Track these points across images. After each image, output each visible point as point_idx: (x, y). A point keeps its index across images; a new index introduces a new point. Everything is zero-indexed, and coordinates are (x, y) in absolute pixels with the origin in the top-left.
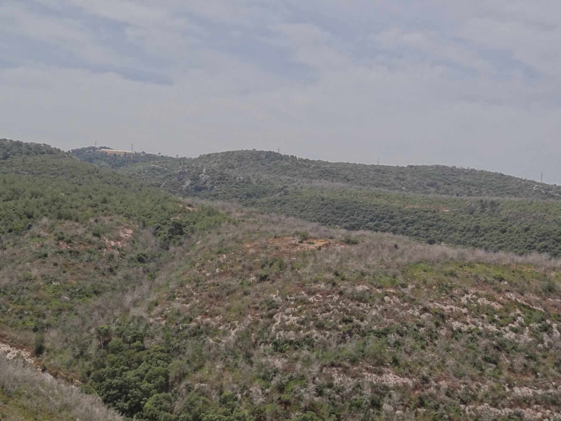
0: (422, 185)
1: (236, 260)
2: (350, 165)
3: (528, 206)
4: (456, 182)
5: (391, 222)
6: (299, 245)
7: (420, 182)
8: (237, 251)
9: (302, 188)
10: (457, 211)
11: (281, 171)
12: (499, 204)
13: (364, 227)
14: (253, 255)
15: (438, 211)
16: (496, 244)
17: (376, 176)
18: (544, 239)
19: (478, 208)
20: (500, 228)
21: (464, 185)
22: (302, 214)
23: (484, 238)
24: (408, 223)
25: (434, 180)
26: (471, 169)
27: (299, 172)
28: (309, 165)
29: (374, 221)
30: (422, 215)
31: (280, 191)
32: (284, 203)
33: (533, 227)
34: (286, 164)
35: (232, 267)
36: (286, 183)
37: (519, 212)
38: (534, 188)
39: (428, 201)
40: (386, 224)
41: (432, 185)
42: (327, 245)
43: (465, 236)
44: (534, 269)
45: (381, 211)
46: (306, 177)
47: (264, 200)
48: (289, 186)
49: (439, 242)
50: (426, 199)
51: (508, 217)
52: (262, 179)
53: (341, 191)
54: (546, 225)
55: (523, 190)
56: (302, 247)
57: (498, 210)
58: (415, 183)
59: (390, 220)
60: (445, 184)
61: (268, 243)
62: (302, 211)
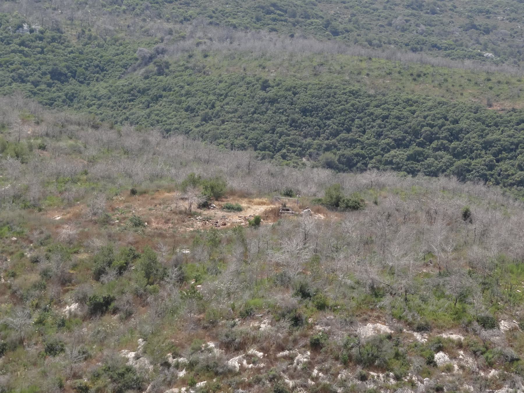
1: (22, 255)
5: (454, 149)
6: (200, 214)
8: (26, 231)
9: (206, 56)
11: (147, 8)
13: (380, 161)
17: (413, 20)
22: (208, 127)
24: (500, 152)
27: (198, 10)
29: (407, 146)
31: (146, 64)
32: (157, 98)
42: (276, 214)
45: (425, 117)
48: (171, 48)
53: (315, 64)
56: (208, 219)
59: (451, 141)
61: (113, 209)
62: (206, 119)
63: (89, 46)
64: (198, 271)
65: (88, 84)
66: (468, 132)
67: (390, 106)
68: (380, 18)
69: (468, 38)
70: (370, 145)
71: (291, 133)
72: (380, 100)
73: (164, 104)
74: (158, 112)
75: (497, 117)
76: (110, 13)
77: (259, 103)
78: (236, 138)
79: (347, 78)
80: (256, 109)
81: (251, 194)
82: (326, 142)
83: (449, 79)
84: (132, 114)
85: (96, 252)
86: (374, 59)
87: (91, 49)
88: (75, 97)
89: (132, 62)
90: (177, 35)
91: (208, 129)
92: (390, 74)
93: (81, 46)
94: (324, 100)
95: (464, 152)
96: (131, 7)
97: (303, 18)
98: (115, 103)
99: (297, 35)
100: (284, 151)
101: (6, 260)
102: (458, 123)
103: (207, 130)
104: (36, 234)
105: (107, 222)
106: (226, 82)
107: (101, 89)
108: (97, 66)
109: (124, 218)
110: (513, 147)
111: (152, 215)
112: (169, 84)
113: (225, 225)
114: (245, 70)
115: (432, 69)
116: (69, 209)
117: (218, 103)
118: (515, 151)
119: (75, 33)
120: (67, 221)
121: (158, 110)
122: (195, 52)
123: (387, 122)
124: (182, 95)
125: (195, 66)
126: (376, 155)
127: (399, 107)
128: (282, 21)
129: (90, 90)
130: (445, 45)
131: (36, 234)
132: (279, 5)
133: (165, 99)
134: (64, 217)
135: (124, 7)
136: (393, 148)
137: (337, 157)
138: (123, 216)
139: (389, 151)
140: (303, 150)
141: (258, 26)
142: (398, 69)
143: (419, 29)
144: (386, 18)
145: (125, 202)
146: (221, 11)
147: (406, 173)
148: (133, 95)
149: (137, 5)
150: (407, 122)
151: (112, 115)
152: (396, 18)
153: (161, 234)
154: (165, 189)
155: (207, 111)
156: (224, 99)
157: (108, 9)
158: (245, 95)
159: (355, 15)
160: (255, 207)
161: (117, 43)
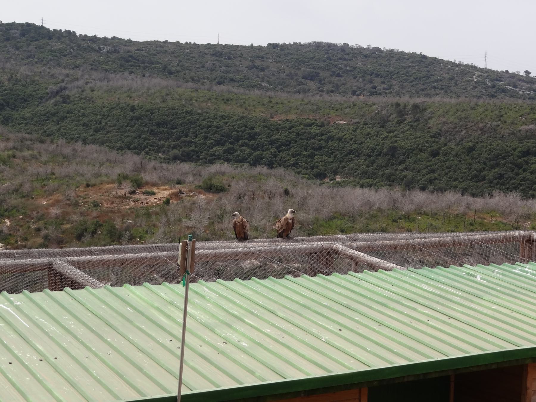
0: (296, 78)
1: (29, 227)
2: (170, 45)
3: (471, 112)
4: (350, 71)
5: (253, 145)
6: (131, 198)
7: (290, 73)
8: (28, 212)
9: (93, 91)
10: (358, 123)
11: (51, 60)
12: (425, 109)
13: (207, 154)
14: (57, 218)
15: (329, 123)
16: (424, 175)
17: (217, 64)
18: (497, 165)
19: (393, 116)
20: (429, 149)
21: (363, 76)
22: (98, 136)
23: (404, 165)
24: (280, 146)
25: (314, 68)
26: (373, 48)
27: (83, 60)
28: (99, 48)
29: (223, 144)
30: (303, 131)
31: (55, 97)
32: (64, 118)
33: (480, 145)
34: (59, 46)
35: (26, 239)
36: (63, 81)
37: (457, 121)
38: (474, 77)
39: (309, 106)
40: (244, 148)
41: (311, 77)
42: (177, 196)
43: (375, 164)
44: (499, 219)
45: (233, 126)
46: (96, 69)
47: (27, 112)
48: (70, 86)
49: (332, 176)
50: (307, 104)
51: (440, 130)
52: (18, 75)
53: (163, 94)
54: (500, 142)
55: (457, 81)
56: (137, 200)
57: (425, 120)
58: (283, 75)
59: (250, 141)
60: (332, 76)
61: (78, 196)
62: (97, 131)
63: (16, 86)
64: (140, 233)
65: (17, 110)
66: (260, 135)
67: (212, 120)
68: (197, 63)
69: (252, 74)
70: (201, 144)
71: (151, 138)
72: (205, 116)
73: (68, 122)
74: (65, 127)
75: (277, 125)
76: (28, 64)
77: (129, 120)
78: (117, 143)
79: (184, 103)
80: (128, 124)
81: (158, 184)
82: (173, 143)
83: (246, 102)
84: (49, 129)
85: (75, 223)
86: (199, 90)
87: (18, 88)
88: (9, 119)
89: (45, 95)
90: (73, 78)
91: (99, 137)
92: (210, 100)
93: (11, 86)
94: (170, 117)
95: (258, 147)
96: (40, 60)
97: (149, 64)
98: (36, 122)
99: (147, 75)
100: (147, 150)
101: (19, 230)
102: (253, 129)
103: (97, 138)
104: (35, 213)
105: (77, 205)
106: (107, 107)
107: (26, 113)
108: (23, 98)
109: (87, 202)
110: (288, 143)
111: (103, 199)
112: (70, 109)
113: (148, 203)
114: (118, 99)
115: (235, 96)
116: (50, 197)
117: (103, 121)
118: (289, 146)
119: (6, 78)
120: (53, 205)
121: (64, 126)
122: (85, 88)
123: (210, 130)
124: (79, 116)
125: (86, 97)
126: (205, 150)
127: (217, 120)
128: (136, 66)
129: (19, 114)
130: (239, 79)
131: (35, 213)
132: (134, 56)
133: (68, 119)
134: (49, 202)
135: (36, 60)
136: (215, 146)
137: (181, 153)
138: (86, 200)
139: (212, 148)
140: (159, 148)
141: (122, 70)
142: (214, 97)
143: (222, 69)
144: (201, 63)
145: (83, 192)
146: (98, 61)
147: (223, 161)
148: (48, 117)
149: (44, 58)
150: (222, 130)
151: (35, 130)
152: (207, 62)
153: (111, 211)
154: (106, 182)
155: (96, 125)
156: (107, 118)
157: (26, 62)
158: (120, 115)
159: (181, 61)
160: (162, 192)
161: (34, 84)
